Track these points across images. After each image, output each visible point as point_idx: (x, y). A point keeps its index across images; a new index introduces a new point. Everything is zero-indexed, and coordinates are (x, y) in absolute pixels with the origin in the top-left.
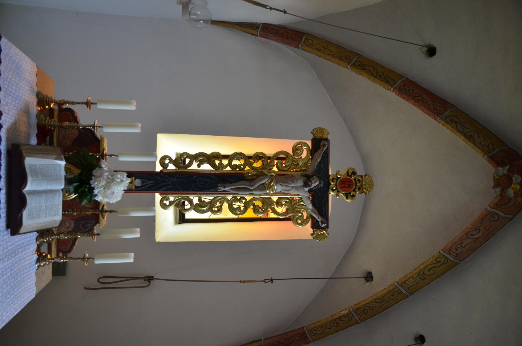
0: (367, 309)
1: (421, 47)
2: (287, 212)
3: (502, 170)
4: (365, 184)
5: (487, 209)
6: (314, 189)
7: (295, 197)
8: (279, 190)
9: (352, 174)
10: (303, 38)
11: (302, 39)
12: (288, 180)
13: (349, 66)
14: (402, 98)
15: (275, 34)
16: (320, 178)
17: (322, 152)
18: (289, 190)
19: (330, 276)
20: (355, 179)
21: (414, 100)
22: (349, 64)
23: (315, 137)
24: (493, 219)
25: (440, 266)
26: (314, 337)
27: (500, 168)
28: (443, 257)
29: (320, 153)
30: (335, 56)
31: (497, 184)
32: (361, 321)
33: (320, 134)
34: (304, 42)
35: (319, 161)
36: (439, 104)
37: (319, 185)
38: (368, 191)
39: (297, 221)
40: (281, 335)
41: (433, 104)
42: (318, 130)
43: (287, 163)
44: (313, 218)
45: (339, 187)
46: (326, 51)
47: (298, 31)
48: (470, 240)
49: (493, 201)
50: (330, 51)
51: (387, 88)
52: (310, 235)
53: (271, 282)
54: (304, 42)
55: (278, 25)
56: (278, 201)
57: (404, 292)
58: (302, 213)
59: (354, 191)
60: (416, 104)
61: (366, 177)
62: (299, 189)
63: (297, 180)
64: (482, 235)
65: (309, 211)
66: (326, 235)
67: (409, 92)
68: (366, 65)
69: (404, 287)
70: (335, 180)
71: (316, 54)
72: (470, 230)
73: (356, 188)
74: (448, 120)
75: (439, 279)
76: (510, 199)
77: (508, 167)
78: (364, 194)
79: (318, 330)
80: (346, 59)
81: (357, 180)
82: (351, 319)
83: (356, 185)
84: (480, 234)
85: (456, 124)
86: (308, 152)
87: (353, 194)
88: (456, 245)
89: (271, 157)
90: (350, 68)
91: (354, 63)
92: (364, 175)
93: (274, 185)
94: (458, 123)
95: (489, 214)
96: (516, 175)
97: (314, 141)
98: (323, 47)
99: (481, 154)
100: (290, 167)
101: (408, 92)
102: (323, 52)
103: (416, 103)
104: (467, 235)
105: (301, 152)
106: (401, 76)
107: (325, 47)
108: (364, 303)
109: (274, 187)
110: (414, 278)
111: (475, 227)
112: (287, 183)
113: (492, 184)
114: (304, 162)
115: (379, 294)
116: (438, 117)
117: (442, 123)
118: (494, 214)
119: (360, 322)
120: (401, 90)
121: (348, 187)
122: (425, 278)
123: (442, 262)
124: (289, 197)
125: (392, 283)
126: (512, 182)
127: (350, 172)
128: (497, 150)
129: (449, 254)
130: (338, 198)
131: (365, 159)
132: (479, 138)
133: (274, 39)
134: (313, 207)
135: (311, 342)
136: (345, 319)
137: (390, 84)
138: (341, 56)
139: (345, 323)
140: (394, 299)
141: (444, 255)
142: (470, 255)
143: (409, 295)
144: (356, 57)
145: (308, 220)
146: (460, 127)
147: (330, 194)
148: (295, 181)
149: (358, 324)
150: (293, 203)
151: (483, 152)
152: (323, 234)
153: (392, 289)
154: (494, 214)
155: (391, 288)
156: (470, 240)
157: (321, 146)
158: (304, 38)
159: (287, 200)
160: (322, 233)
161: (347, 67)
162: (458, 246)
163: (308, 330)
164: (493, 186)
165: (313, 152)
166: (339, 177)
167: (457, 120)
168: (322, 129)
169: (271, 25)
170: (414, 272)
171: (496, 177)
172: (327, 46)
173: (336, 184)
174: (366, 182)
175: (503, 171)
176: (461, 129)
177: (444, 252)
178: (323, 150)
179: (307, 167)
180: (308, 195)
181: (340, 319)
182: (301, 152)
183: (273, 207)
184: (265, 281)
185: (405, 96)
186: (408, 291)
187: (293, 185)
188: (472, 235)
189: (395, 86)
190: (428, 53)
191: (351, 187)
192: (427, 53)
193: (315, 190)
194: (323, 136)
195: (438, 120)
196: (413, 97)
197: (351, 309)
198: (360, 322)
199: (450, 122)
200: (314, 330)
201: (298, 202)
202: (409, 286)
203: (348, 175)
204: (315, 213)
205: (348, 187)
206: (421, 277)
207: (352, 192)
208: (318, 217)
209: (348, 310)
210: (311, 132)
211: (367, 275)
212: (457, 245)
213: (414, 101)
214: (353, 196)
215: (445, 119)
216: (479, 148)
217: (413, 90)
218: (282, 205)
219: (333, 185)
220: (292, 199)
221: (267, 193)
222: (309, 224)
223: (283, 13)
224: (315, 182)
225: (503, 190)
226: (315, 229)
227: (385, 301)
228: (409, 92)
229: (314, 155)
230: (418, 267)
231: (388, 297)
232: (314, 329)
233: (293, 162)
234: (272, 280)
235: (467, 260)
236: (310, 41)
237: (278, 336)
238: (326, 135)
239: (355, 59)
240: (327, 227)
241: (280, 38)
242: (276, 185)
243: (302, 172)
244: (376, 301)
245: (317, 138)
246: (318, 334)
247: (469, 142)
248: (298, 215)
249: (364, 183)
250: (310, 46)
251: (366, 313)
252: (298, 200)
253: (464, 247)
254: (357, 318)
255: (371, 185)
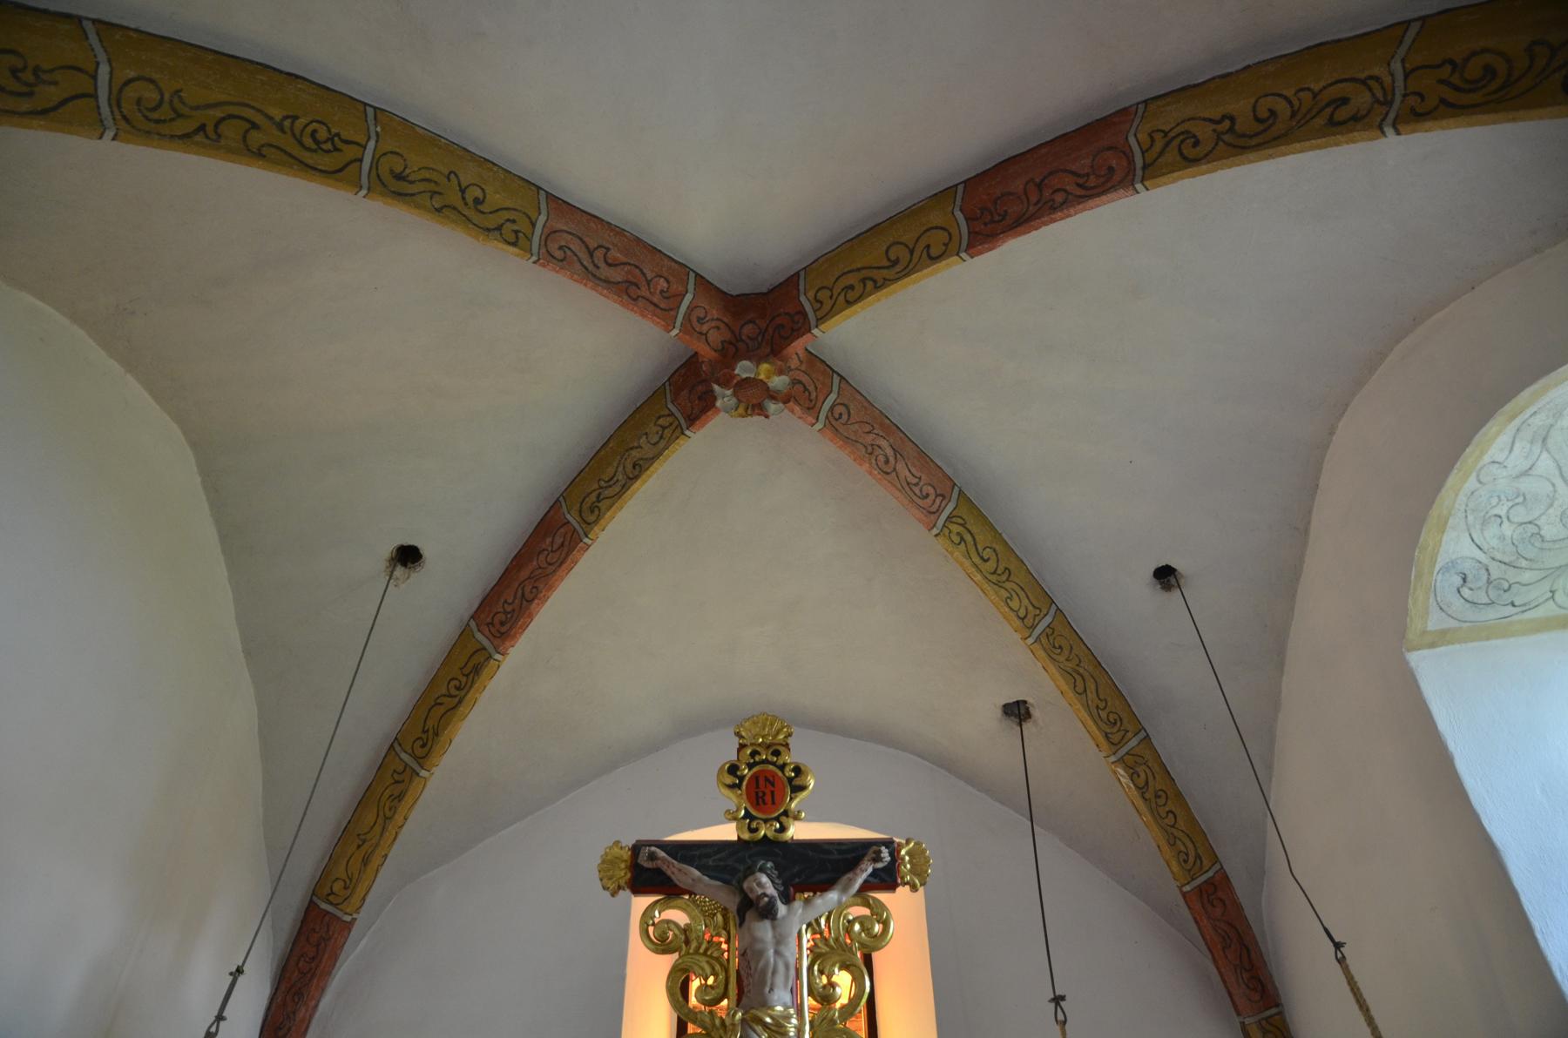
0: (1106, 716)
1: (392, 581)
2: (852, 968)
3: (723, 398)
4: (763, 737)
5: (820, 430)
6: (782, 889)
7: (805, 945)
8: (787, 998)
9: (736, 776)
10: (325, 910)
11: (328, 913)
12: (756, 969)
13: (423, 773)
14: (524, 630)
15: (299, 1000)
16: (750, 871)
17: (673, 863)
18: (787, 967)
19: (1025, 820)
20: (750, 766)
21: (533, 599)
22: (418, 774)
23: (626, 883)
24: (845, 417)
25: (971, 534)
26: (1205, 862)
27: (718, 404)
28: (947, 527)
29: (676, 871)
30: (388, 814)
31: (758, 409)
32: (1140, 731)
33: (619, 867)
34: (338, 904)
35: (697, 873)
36: (548, 540)
37: (769, 872)
38: (783, 727)
39: (876, 936)
40: (1215, 961)
41: (546, 552)
42: (608, 874)
43: (703, 969)
44: (867, 887)
45: (774, 812)
46: (371, 839)
47: (299, 924)
48: (900, 466)
49: (800, 418)
50: (372, 828)
51: (495, 668)
52: (915, 894)
53: (1062, 1003)
54: (336, 905)
55: (272, 986)
56: (818, 998)
57: (1048, 619)
58: (855, 919)
59: (782, 767)
60: (544, 596)
61: (743, 734)
62: (780, 935)
63: (755, 940)
64: (884, 438)
65: (844, 899)
66: (912, 845)
67: (509, 613)
68: (424, 727)
69: (1036, 622)
70: (754, 825)
71: (377, 871)
72: (876, 467)
73: (774, 764)
74: (591, 518)
75: (1004, 535)
76: (795, 382)
77: (716, 387)
78: (790, 740)
79: (1183, 848)
80: (403, 781)
81: (752, 761)
82: (1140, 756)
83: (766, 762)
84: (884, 443)
85: (604, 499)
86: (672, 904)
87: (793, 770)
88: (914, 498)
89: (679, 1018)
90: (429, 771)
91: (416, 758)
92: (737, 738)
93: (773, 1013)
94: (599, 494)
95: (833, 426)
96: (736, 372)
97: (638, 887)
98: (359, 847)
99: (682, 442)
100: (717, 959)
101: (509, 616)
102: (372, 848)
103: (542, 595)
104: (887, 473)
105: (672, 926)
106: (465, 634)
107: (361, 843)
108: (1090, 723)
109: (779, 1014)
110: (1009, 595)
111: (867, 455)
112: (764, 972)
113: (756, 419)
114: (702, 918)
115: (1062, 682)
116: (581, 541)
117: (598, 531)
118: (832, 413)
119: (1143, 731)
120: (504, 633)
121: (773, 785)
122: (1006, 569)
123: (961, 529)
124: (805, 963)
125: (1030, 652)
126: (754, 378)
127: (729, 780)
128: (674, 409)
129: (939, 511)
130: (803, 814)
131: (689, 728)
132: (641, 447)
133: (313, 1003)
134: (834, 889)
135: (1222, 868)
136: (1143, 775)
137: (485, 661)
138: (390, 796)
139: (1153, 774)
140: (1070, 644)
141: (944, 526)
142: (937, 465)
143: (1053, 608)
144: (399, 752)
145: (871, 902)
146: (611, 489)
147: (794, 838)
148: (758, 946)
149: (1151, 737)
150: (824, 949)
151: (678, 438)
152: (910, 856)
153: (1045, 650)
154: (832, 413)
155: (1041, 653)
156: (900, 466)
157: (655, 866)
158: (324, 906)
159: (816, 968)
160: (907, 858)
161: (425, 778)
162: (917, 492)
163: (1190, 879)
164: (763, 418)
165: (668, 889)
166: (743, 812)
167: (593, 497)
168: (603, 862)
169: (268, 1009)
170: (993, 597)
171: (741, 410)
172: (359, 835)
173: (766, 821)
174: (756, 735)
175: (725, 397)
176: (617, 489)
177: (934, 526)
178: (666, 860)
179: (715, 909)
180: (798, 905)
181: (1143, 788)
182: (672, 926)
183: (837, 1014)
184: (1061, 1021)
185: (520, 623)
186: (1045, 611)
187: (771, 952)
188: (887, 462)
189: (491, 649)
190: (409, 565)
191: (773, 777)
192: (410, 568)
193: (783, 884)
194: (626, 861)
195: (590, 542)
196: (525, 602)
197: (1113, 759)
198: (1143, 731)
199: (597, 512)
200: (1186, 862)
201: (821, 933)
202: (1030, 608)
203: (739, 786)
204: (851, 881)
205: (773, 785)
206: (1004, 578)
207: (787, 774)
208: (863, 871)
209: (1115, 767)
210: (613, 895)
211: (1013, 718)
212: (915, 494)
213: (536, 601)
214: (798, 770)
215: (589, 524)
216: (666, 448)
217: (506, 602)
218: (832, 985)
219: (767, 829)
220: (811, 951)
221: (795, 1035)
222: (882, 897)
223: (241, 979)
224: (760, 884)
225: (773, 396)
226: (896, 881)
227: (1077, 668)
228: (509, 613)
229: (681, 889)
230: (978, 585)
231: (1067, 660)
232: (1183, 864)
233: (701, 951)
234: (1058, 1000)
235: (949, 472)
236: (337, 887)
237: (1223, 970)
238: (622, 852)
239: (404, 756)
240: (888, 843)
241: (315, 981)
242: (772, 1008)
243: (732, 923)
244: (1081, 690)
245: (629, 879)
246: (1196, 850)
247: (652, 469)
248: (860, 934)
249: (761, 740)
250: (351, 887)
251: (1116, 717)
252: (814, 933)
253: (917, 480)
254: (1133, 742)
255: (766, 719)
